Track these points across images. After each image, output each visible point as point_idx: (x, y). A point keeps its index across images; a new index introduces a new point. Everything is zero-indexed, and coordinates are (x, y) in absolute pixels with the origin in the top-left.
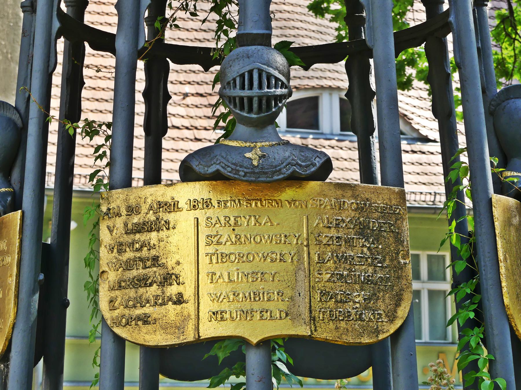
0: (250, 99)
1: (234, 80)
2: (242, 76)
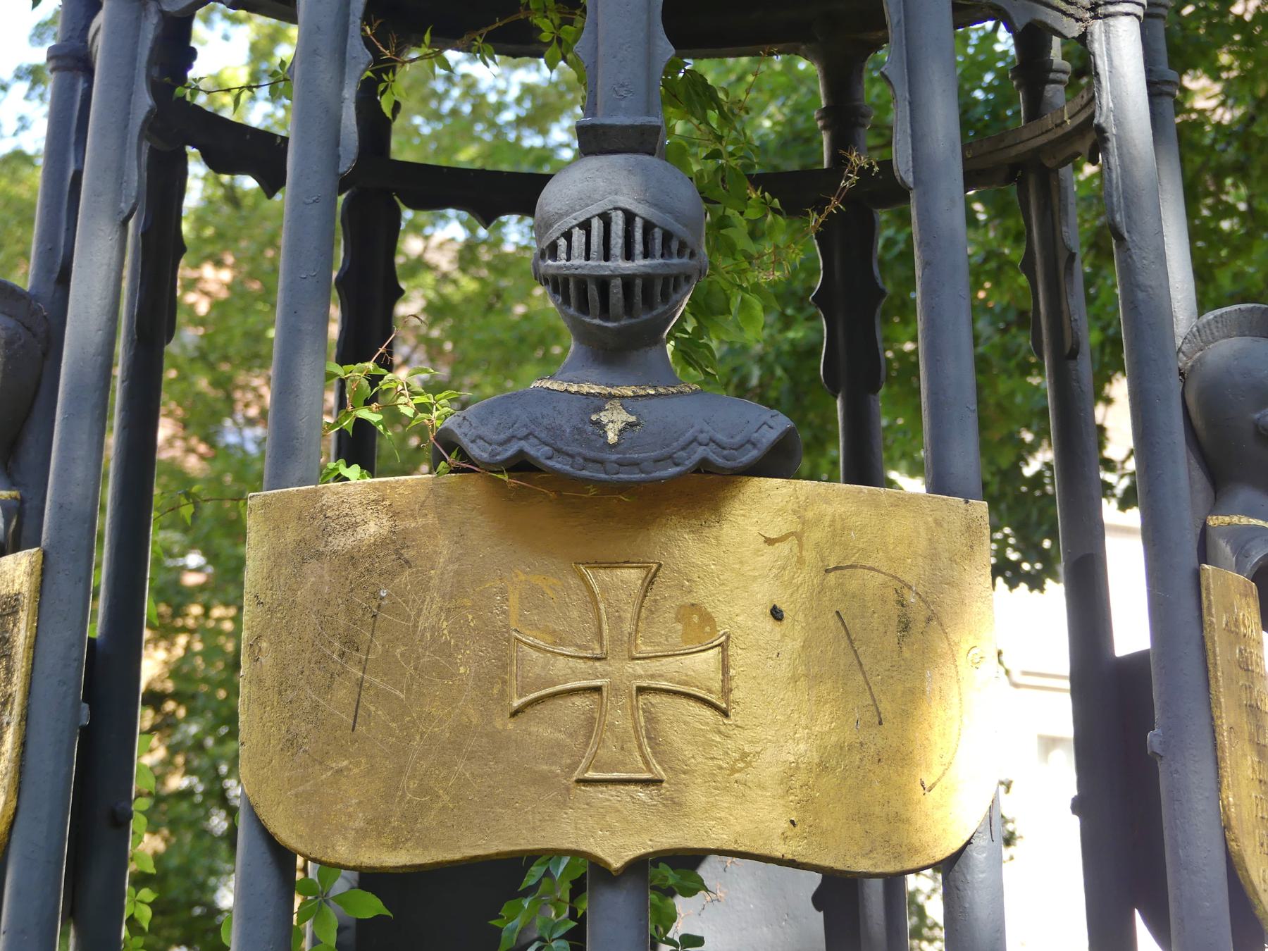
0: (603, 283)
1: (568, 235)
2: (586, 226)
